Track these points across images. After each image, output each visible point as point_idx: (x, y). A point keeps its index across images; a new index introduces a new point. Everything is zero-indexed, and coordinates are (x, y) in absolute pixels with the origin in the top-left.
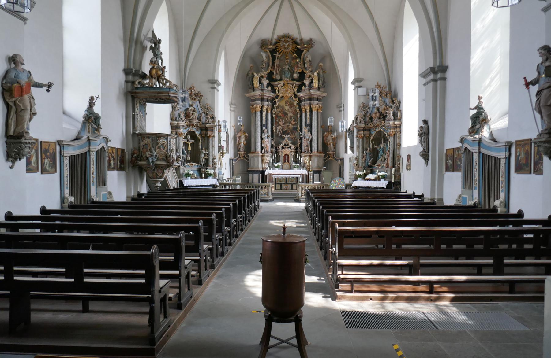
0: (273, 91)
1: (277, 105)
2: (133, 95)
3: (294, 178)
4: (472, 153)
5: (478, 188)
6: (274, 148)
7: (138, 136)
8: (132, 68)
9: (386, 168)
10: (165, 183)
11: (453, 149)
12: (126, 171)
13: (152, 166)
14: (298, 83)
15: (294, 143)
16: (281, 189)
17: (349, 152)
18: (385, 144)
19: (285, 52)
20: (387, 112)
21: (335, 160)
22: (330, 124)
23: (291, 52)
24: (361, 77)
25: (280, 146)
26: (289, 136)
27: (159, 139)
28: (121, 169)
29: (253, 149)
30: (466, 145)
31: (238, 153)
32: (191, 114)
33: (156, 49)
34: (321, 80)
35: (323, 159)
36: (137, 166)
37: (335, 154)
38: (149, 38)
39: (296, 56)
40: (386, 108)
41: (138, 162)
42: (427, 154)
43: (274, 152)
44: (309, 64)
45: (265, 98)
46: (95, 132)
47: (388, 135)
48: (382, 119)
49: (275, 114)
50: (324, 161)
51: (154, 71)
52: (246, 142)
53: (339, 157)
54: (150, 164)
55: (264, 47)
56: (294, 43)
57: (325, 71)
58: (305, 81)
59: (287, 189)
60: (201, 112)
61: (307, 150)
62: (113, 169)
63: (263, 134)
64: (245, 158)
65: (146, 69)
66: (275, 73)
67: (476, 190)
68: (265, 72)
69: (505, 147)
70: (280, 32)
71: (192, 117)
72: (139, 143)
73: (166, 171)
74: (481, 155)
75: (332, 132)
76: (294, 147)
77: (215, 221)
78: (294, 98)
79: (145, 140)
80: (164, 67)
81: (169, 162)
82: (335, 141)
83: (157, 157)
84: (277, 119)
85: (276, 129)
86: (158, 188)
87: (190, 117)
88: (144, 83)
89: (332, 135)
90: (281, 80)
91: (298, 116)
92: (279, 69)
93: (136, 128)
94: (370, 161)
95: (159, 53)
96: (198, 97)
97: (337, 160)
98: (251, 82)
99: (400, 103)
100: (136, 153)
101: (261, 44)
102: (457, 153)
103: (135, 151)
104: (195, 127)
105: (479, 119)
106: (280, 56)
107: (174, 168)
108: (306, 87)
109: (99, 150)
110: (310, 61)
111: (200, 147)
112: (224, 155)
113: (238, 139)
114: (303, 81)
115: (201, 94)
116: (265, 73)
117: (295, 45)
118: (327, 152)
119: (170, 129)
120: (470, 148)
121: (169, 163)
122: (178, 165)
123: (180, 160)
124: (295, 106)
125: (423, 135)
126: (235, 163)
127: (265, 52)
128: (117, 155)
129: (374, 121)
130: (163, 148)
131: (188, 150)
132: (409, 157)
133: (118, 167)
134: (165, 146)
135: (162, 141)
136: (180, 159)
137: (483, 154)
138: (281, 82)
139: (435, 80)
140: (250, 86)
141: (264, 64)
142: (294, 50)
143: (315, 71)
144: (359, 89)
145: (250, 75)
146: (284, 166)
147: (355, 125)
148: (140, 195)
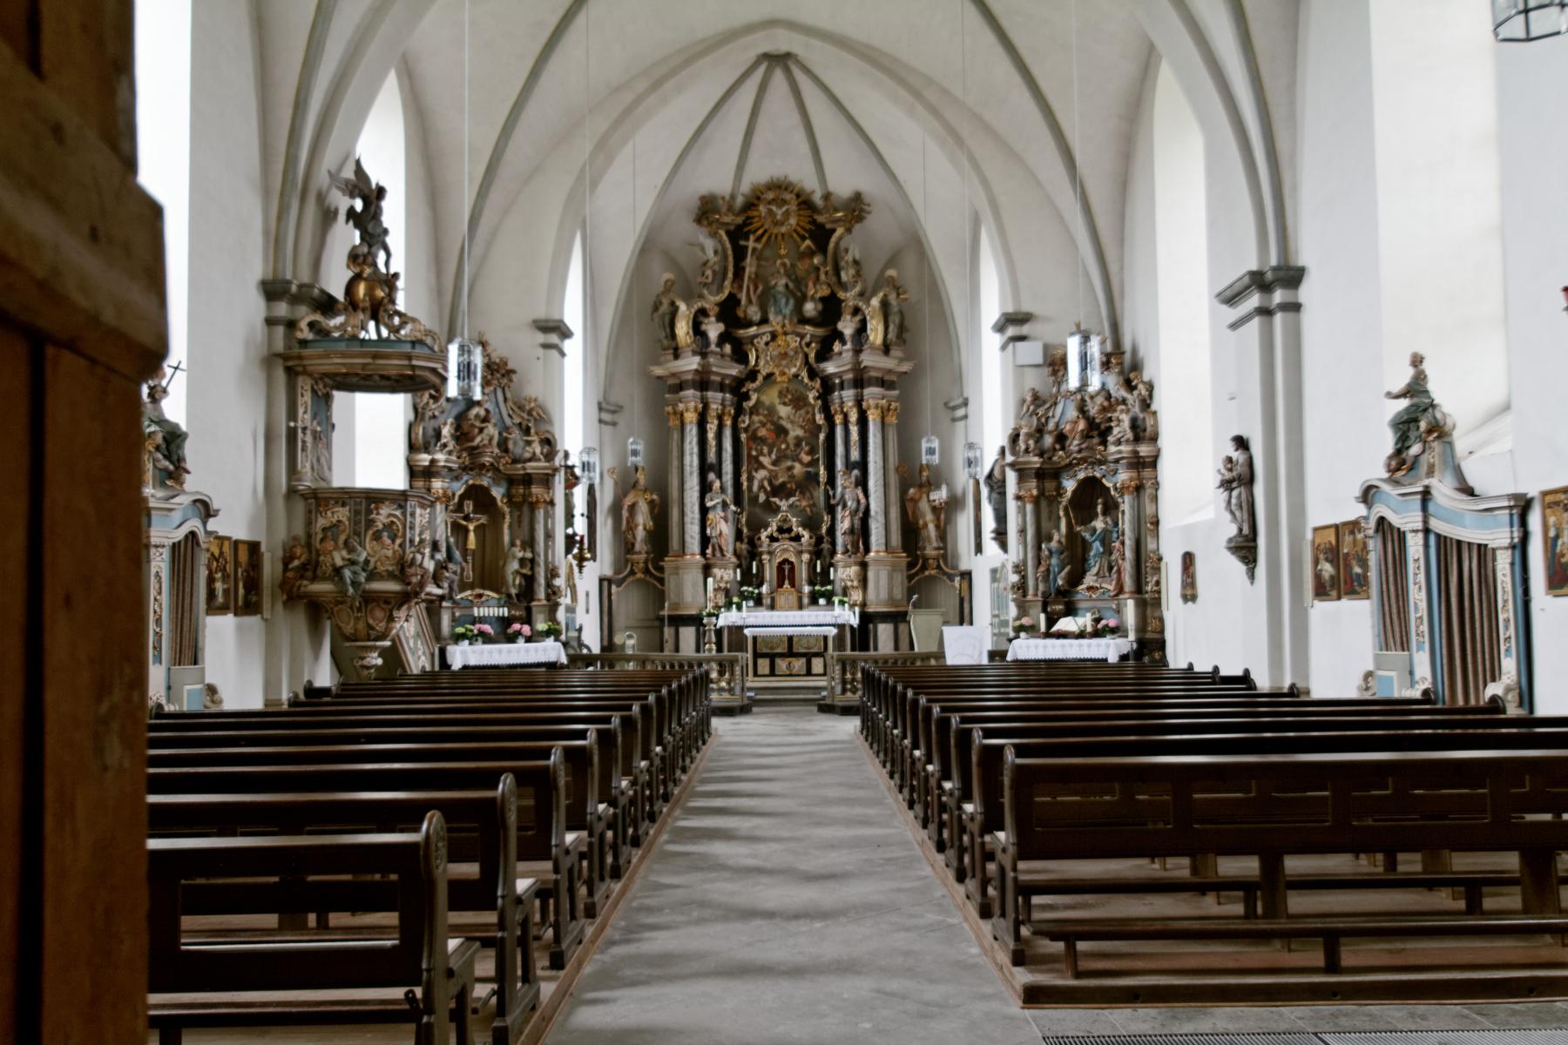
0: (740, 356)
1: (752, 403)
2: (290, 363)
3: (817, 637)
4: (1404, 533)
5: (1427, 646)
6: (746, 540)
7: (306, 499)
8: (289, 276)
9: (1117, 595)
10: (394, 656)
11: (1336, 527)
12: (262, 618)
13: (353, 599)
14: (820, 332)
15: (811, 523)
16: (772, 673)
17: (990, 546)
18: (1108, 519)
19: (776, 236)
20: (1111, 418)
21: (945, 578)
22: (929, 457)
23: (795, 235)
24: (1027, 307)
25: (764, 535)
26: (792, 500)
27: (377, 508)
28: (249, 607)
29: (674, 543)
30: (1380, 510)
31: (627, 561)
32: (476, 431)
33: (370, 217)
34: (894, 322)
35: (905, 574)
36: (300, 597)
37: (944, 557)
38: (347, 182)
39: (813, 247)
40: (1106, 404)
41: (306, 586)
42: (1252, 544)
43: (745, 553)
44: (852, 272)
45: (714, 382)
46: (168, 483)
47: (1116, 489)
48: (1096, 440)
49: (746, 430)
50: (910, 581)
51: (361, 289)
52: (651, 524)
53: (955, 567)
54: (347, 590)
55: (707, 218)
56: (803, 206)
57: (905, 293)
58: (840, 326)
59: (794, 672)
60: (508, 422)
61: (853, 546)
62: (223, 609)
63: (708, 496)
64: (652, 575)
65: (335, 281)
66: (744, 301)
67: (1421, 652)
68: (712, 298)
69: (1507, 511)
70: (760, 172)
71: (478, 440)
72: (309, 523)
73: (402, 613)
74: (1432, 539)
75: (931, 484)
76: (811, 537)
77: (513, 808)
78: (806, 380)
79: (329, 513)
80: (396, 276)
81: (409, 584)
82: (942, 517)
83: (372, 565)
84: (754, 446)
85: (750, 479)
86: (373, 671)
87: (472, 440)
88: (328, 325)
89: (932, 498)
90: (764, 321)
91: (822, 436)
92: (756, 288)
93: (300, 472)
94: (1063, 574)
95: (379, 231)
96: (499, 375)
97: (951, 578)
98: (668, 330)
99: (1150, 387)
100: (298, 554)
101: (699, 209)
102: (1348, 539)
103: (294, 550)
104: (489, 474)
105: (1418, 428)
106: (759, 246)
107: (423, 605)
108: (844, 342)
109: (179, 542)
110: (856, 262)
111: (506, 538)
112: (585, 563)
113: (625, 514)
114: (835, 323)
115: (510, 366)
116: (711, 301)
117: (808, 213)
118: (919, 553)
119: (408, 478)
120: (1395, 519)
121: (409, 588)
122: (439, 591)
123: (447, 578)
124: (810, 404)
125: (1234, 485)
126: (618, 592)
127: (714, 235)
128: (237, 563)
129: (1072, 447)
130: (389, 537)
131: (467, 550)
132: (1188, 560)
133: (240, 603)
134: (398, 530)
135: (384, 514)
136: (447, 574)
137: (1438, 536)
138: (766, 329)
139: (1265, 312)
140: (666, 342)
141: (709, 272)
142: (803, 228)
143: (874, 294)
144: (1019, 345)
145: (665, 307)
146: (777, 598)
147: (1009, 458)
148: (312, 692)
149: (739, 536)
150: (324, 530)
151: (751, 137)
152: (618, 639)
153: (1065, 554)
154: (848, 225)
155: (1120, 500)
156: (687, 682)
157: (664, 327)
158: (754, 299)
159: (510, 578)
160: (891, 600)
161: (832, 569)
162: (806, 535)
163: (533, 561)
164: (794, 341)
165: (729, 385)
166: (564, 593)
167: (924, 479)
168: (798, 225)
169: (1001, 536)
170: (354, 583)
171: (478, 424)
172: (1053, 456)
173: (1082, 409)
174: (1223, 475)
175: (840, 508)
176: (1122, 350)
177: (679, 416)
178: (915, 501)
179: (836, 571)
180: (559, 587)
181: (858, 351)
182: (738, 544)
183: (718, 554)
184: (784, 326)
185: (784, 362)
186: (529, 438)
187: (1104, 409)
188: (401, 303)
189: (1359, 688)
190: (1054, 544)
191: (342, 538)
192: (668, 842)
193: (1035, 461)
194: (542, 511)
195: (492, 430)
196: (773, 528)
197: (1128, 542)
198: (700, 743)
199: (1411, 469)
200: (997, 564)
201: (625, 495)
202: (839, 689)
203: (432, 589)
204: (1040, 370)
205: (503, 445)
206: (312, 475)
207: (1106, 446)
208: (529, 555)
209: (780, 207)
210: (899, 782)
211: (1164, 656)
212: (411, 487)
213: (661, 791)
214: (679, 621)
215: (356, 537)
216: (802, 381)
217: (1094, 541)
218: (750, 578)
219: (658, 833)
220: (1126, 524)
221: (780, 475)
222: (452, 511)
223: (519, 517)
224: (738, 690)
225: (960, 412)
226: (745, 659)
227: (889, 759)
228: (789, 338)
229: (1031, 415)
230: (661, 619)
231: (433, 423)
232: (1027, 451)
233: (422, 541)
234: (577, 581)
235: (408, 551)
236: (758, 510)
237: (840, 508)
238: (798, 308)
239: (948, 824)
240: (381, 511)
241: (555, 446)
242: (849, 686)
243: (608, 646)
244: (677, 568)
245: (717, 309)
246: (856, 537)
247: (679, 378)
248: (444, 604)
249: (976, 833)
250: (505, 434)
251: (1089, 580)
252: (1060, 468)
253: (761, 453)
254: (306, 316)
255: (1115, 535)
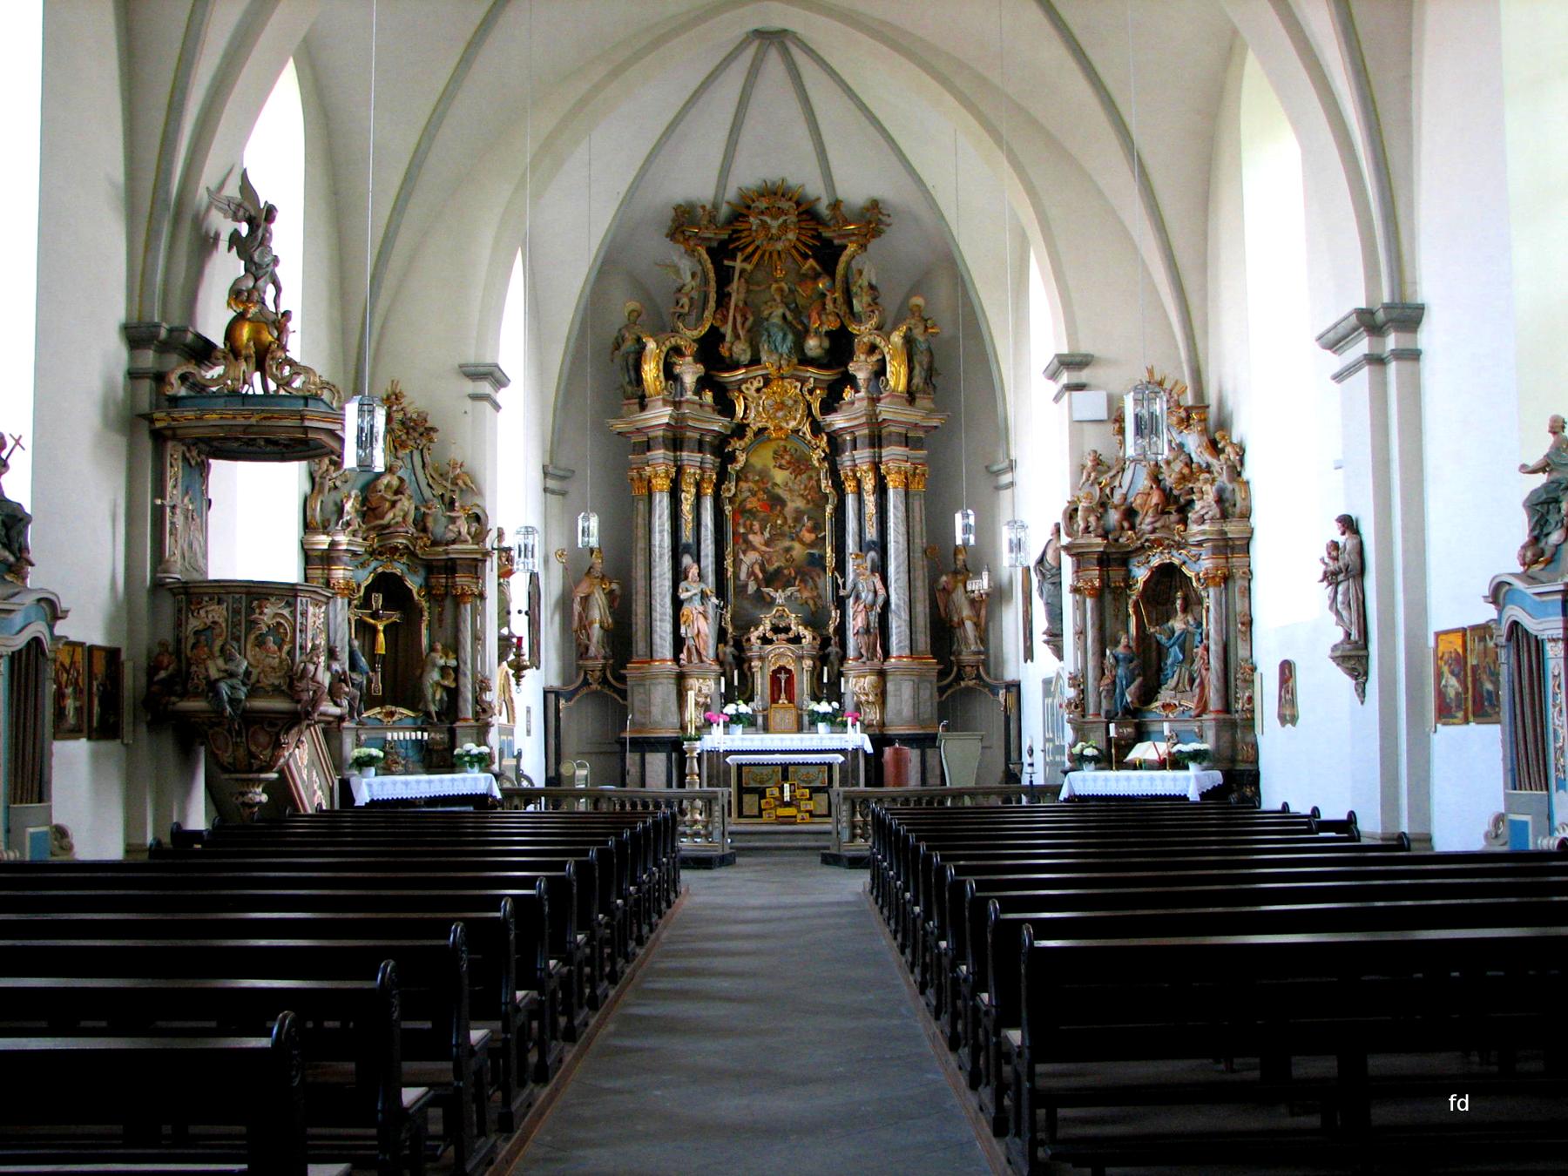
0: (725, 406)
1: (738, 466)
6: (731, 643)
7: (175, 595)
10: (283, 791)
11: (1464, 630)
12: (122, 742)
13: (232, 719)
14: (827, 375)
15: (815, 621)
20: (1192, 488)
24: (1085, 348)
25: (754, 636)
26: (790, 590)
27: (260, 607)
29: (640, 646)
30: (1514, 612)
32: (387, 505)
33: (257, 243)
37: (985, 663)
38: (229, 201)
40: (1186, 471)
41: (174, 704)
42: (1362, 653)
43: (730, 658)
44: (866, 299)
46: (8, 578)
47: (1198, 580)
48: (1174, 517)
49: (731, 500)
50: (941, 696)
51: (245, 332)
53: (999, 677)
54: (224, 709)
55: (683, 232)
56: (804, 217)
58: (852, 368)
60: (427, 493)
61: (867, 651)
62: (74, 733)
63: (683, 585)
64: (610, 686)
65: (213, 322)
66: (728, 338)
67: (1561, 791)
68: (688, 333)
70: (749, 174)
72: (179, 625)
73: (291, 738)
75: (966, 572)
76: (814, 638)
78: (808, 437)
80: (287, 314)
81: (299, 701)
82: (983, 612)
83: (253, 678)
84: (741, 521)
85: (737, 563)
87: (382, 518)
88: (203, 377)
89: (969, 588)
91: (829, 509)
92: (745, 319)
95: (268, 259)
96: (416, 435)
97: (994, 691)
98: (632, 373)
99: (1241, 451)
101: (674, 221)
103: (161, 658)
104: (404, 560)
106: (749, 267)
109: (20, 651)
110: (872, 287)
111: (425, 641)
113: (577, 608)
114: (846, 365)
116: (689, 336)
117: (812, 225)
118: (952, 658)
119: (302, 565)
120: (1530, 624)
121: (299, 707)
122: (337, 711)
123: (346, 694)
124: (814, 467)
125: (1341, 577)
127: (691, 253)
128: (91, 676)
129: (1143, 526)
132: (1287, 670)
135: (270, 613)
140: (629, 389)
141: (685, 301)
143: (895, 327)
144: (1076, 394)
145: (629, 345)
148: (182, 837)
149: (721, 635)
150: (197, 633)
151: (740, 129)
152: (566, 769)
153: (1135, 663)
154: (862, 241)
155: (1204, 594)
156: (645, 829)
157: (628, 371)
158: (741, 333)
159: (430, 692)
160: (917, 718)
161: (842, 679)
162: (807, 635)
163: (456, 670)
164: (793, 388)
165: (710, 443)
166: (496, 711)
167: (960, 563)
168: (798, 239)
169: (1054, 638)
170: (232, 701)
171: (389, 496)
172: (1121, 536)
173: (1156, 479)
174: (1326, 564)
175: (851, 600)
176: (1206, 403)
177: (646, 483)
178: (947, 592)
179: (847, 682)
180: (490, 703)
181: (874, 401)
182: (721, 646)
183: (695, 658)
184: (780, 367)
185: (780, 414)
186: (453, 514)
187: (1183, 478)
188: (295, 347)
189: (1487, 836)
190: (1120, 650)
191: (219, 643)
192: (616, 1034)
193: (1097, 543)
194: (469, 606)
195: (406, 504)
196: (765, 627)
197: (1212, 647)
198: (664, 905)
199: (1550, 561)
200: (1051, 674)
201: (577, 583)
202: (846, 835)
203: (329, 708)
204: (1101, 426)
205: (421, 523)
206: (183, 565)
207: (1186, 525)
208: (453, 663)
209: (775, 218)
210: (910, 959)
211: (1258, 793)
212: (306, 579)
213: (607, 969)
214: (645, 745)
215: (235, 644)
216: (804, 437)
217: (1171, 647)
218: (741, 689)
219: (600, 1025)
220: (1211, 626)
221: (774, 558)
222: (356, 607)
223: (441, 614)
224: (717, 834)
225: (1006, 479)
226: (726, 795)
227: (900, 929)
228: (786, 383)
229: (1092, 484)
230: (622, 743)
231: (336, 496)
232: (1087, 530)
233: (314, 647)
234: (514, 695)
235: (298, 659)
236: (747, 604)
237: (851, 600)
238: (799, 347)
239: (963, 1015)
240: (266, 610)
241: (486, 525)
242: (859, 831)
243: (553, 779)
244: (643, 678)
245: (695, 347)
246: (871, 638)
247: (646, 434)
248: (346, 724)
249: (991, 1028)
250: (423, 509)
251: (1165, 695)
252: (1130, 552)
253: (751, 530)
254: (176, 367)
255: (1198, 638)
